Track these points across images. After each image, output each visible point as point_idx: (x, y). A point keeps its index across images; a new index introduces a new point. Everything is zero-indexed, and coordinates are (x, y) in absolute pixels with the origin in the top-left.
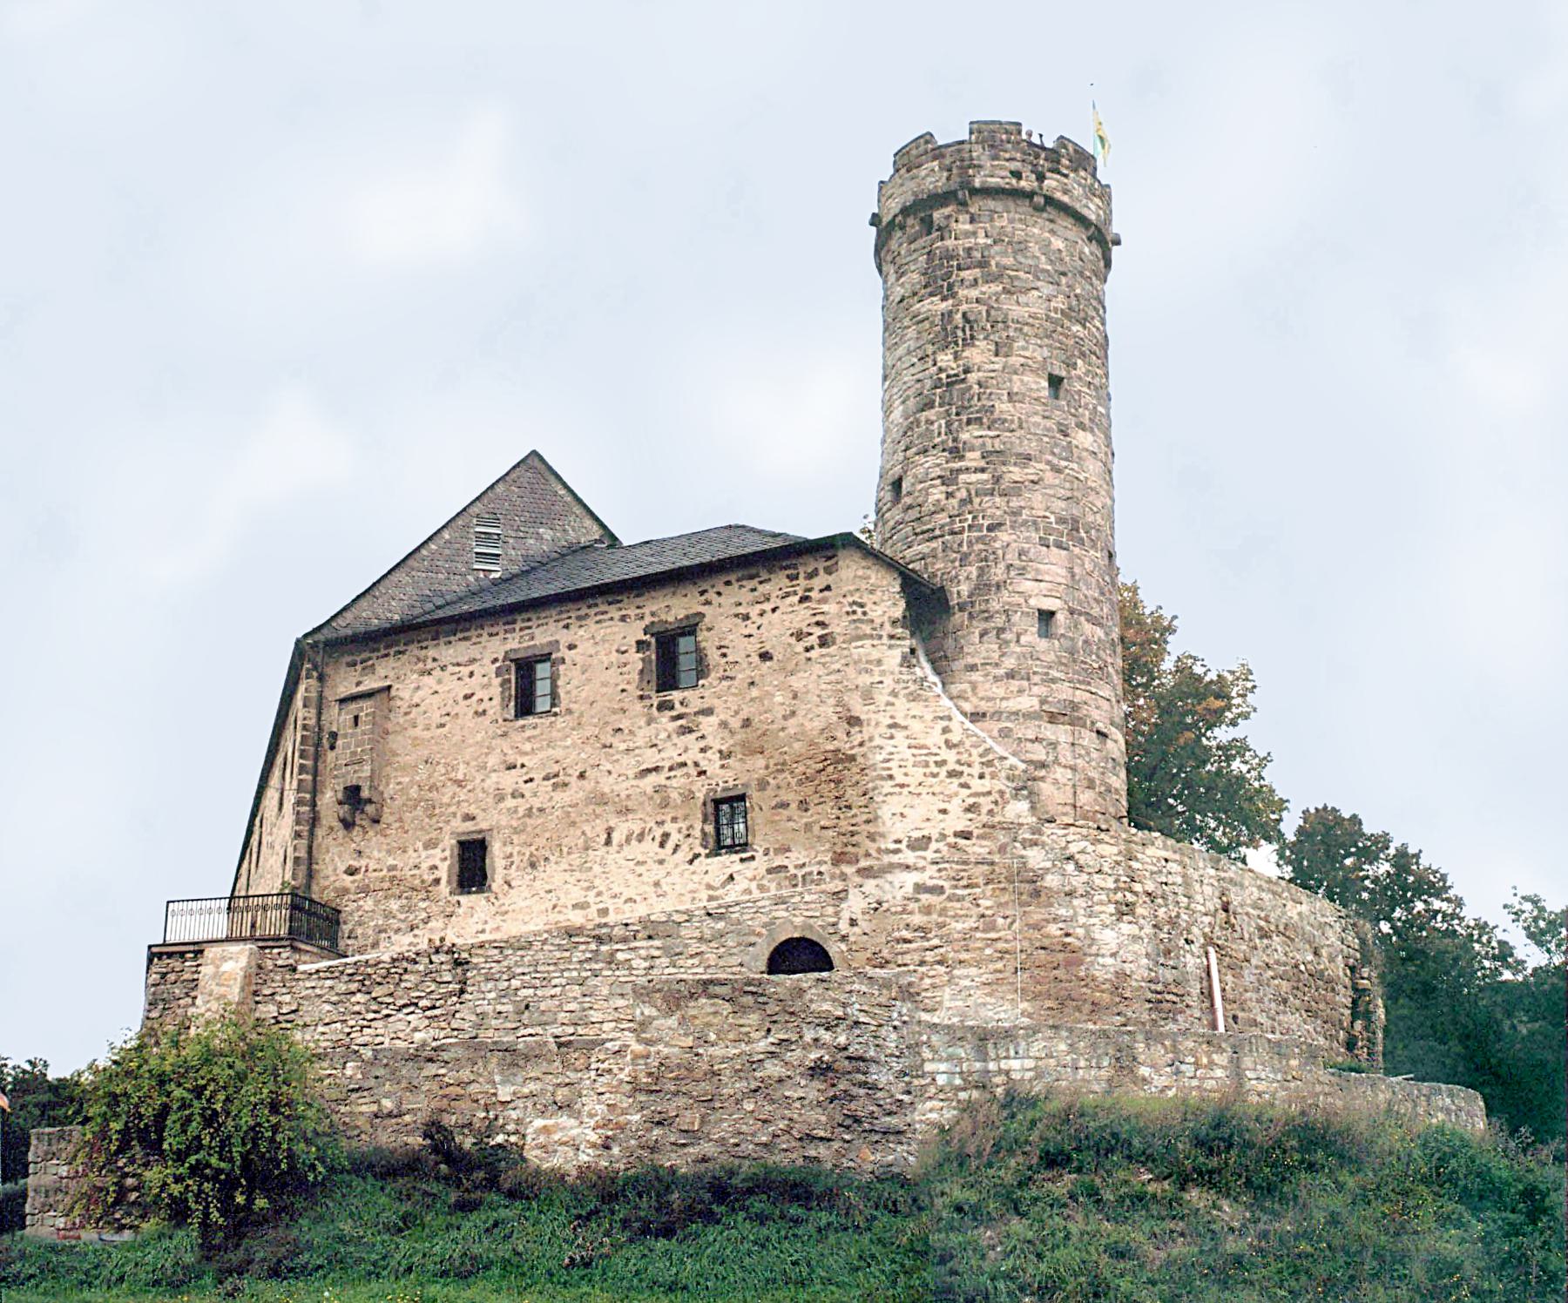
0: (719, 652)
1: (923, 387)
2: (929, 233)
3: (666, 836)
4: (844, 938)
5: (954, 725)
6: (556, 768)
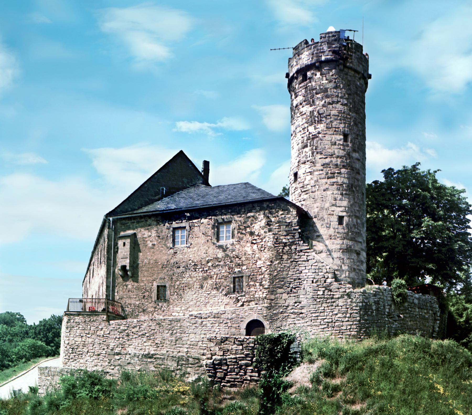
1: (304, 140)
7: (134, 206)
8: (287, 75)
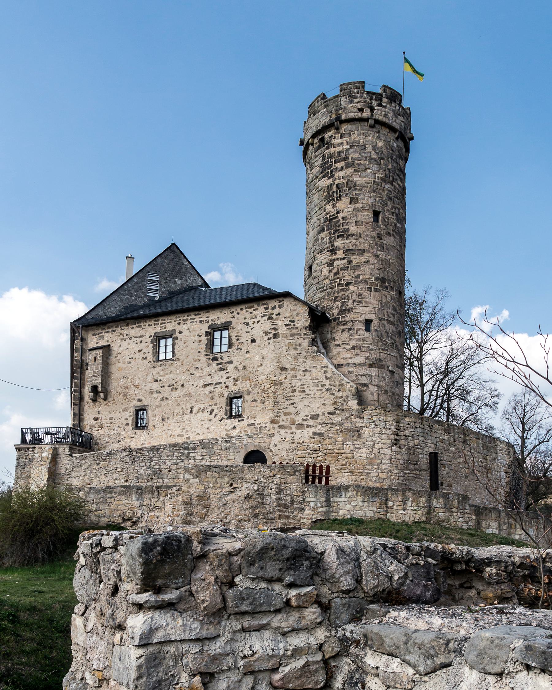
0: (237, 338)
1: (320, 222)
2: (324, 146)
3: (213, 410)
4: (271, 451)
5: (329, 370)
6: (173, 382)
7: (111, 312)
8: (302, 143)
